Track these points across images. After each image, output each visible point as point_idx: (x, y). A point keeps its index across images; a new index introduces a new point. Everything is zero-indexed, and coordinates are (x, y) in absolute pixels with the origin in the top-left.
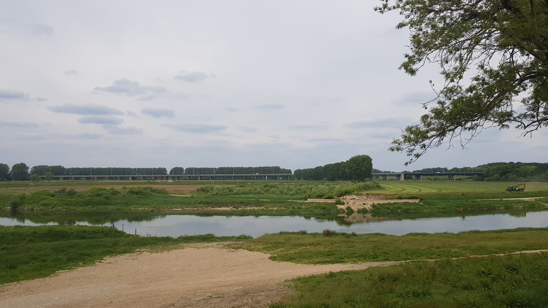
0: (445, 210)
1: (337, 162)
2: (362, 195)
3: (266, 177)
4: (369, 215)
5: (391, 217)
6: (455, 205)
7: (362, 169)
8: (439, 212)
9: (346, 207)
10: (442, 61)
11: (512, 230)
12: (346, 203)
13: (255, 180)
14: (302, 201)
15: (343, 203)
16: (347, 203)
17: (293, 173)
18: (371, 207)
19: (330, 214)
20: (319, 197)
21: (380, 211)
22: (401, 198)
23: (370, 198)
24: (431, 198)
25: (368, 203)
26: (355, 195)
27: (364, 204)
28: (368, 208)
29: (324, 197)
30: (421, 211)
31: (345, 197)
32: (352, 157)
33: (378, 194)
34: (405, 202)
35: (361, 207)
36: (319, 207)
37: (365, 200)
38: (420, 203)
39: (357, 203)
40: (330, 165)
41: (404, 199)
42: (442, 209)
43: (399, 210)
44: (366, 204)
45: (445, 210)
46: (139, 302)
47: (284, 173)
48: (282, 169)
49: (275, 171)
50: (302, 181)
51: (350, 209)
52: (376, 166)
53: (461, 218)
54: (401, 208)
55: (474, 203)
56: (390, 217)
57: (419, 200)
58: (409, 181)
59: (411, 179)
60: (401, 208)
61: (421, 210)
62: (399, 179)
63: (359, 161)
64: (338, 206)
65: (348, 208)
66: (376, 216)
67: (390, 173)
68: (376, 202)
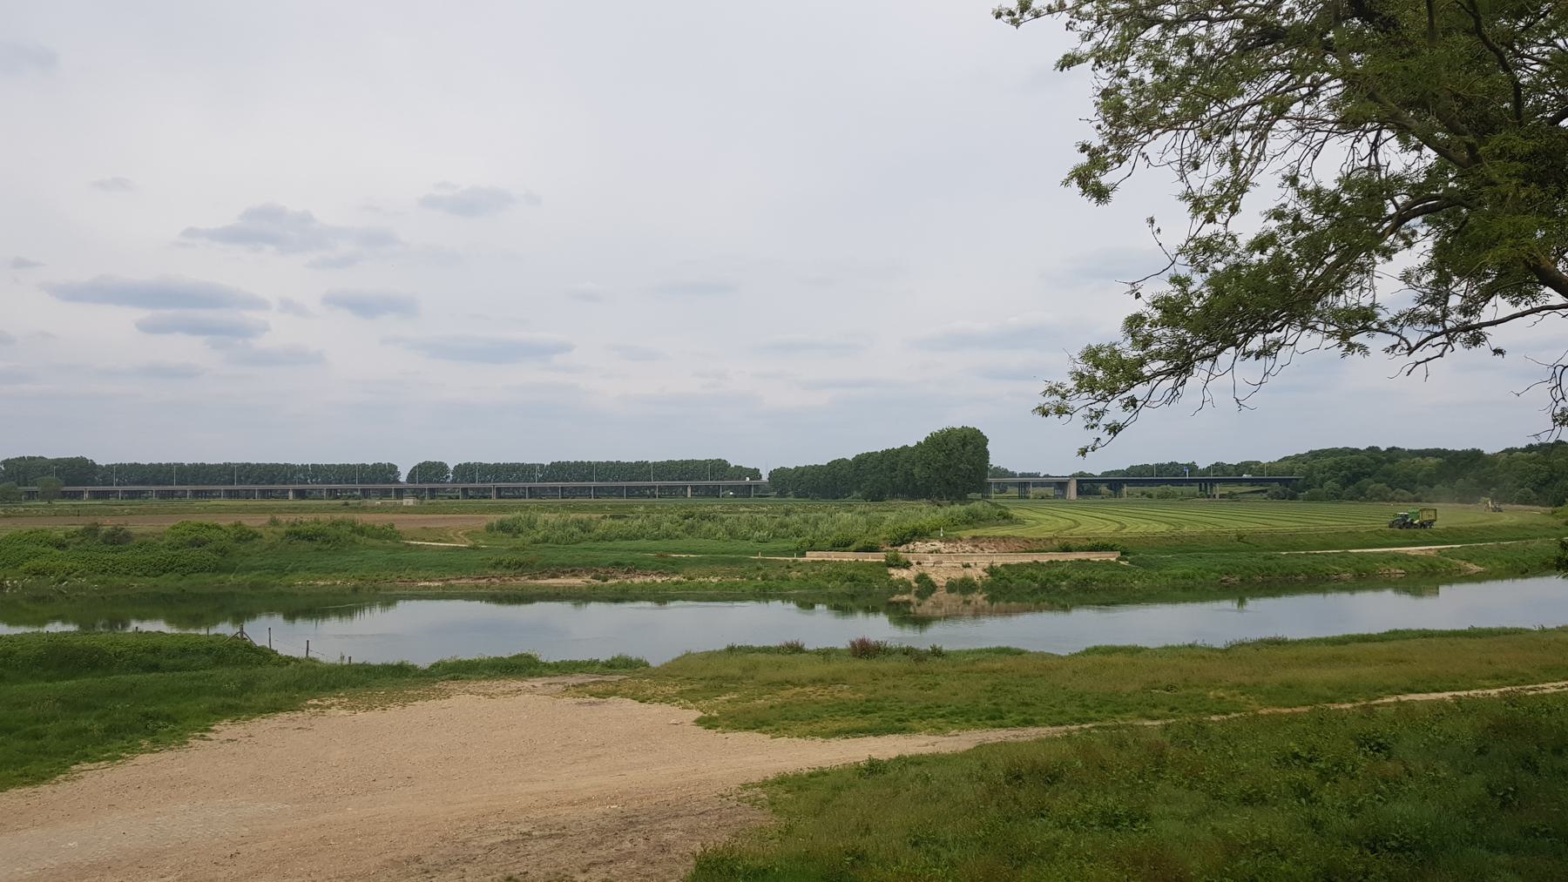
0: (1191, 583)
2: (961, 539)
3: (689, 490)
4: (978, 598)
7: (961, 466)
8: (1175, 588)
9: (916, 574)
12: (914, 562)
15: (908, 562)
16: (919, 563)
17: (765, 478)
18: (986, 574)
19: (870, 595)
20: (839, 546)
22: (1067, 549)
23: (982, 549)
25: (976, 564)
28: (975, 578)
29: (852, 547)
31: (911, 546)
33: (1004, 537)
34: (1079, 560)
35: (958, 575)
37: (968, 554)
38: (1122, 563)
39: (946, 563)
40: (869, 455)
41: (1077, 550)
42: (1183, 578)
43: (1064, 583)
44: (969, 567)
48: (732, 466)
50: (791, 501)
52: (1001, 456)
54: (1067, 577)
55: (1270, 563)
57: (1118, 554)
59: (1095, 494)
60: (1067, 577)
61: (1124, 581)
62: (1063, 496)
64: (892, 571)
65: (921, 578)
66: (998, 600)
68: (999, 561)
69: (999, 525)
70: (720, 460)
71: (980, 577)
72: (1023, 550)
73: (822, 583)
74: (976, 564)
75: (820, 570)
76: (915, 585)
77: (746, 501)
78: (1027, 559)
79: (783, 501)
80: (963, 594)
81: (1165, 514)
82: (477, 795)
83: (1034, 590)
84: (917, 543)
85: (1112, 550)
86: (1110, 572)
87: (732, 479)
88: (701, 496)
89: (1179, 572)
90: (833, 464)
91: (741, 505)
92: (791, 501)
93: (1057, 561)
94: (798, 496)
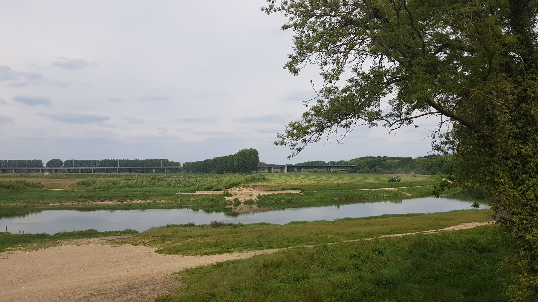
0: (323, 200)
1: (226, 156)
3: (154, 170)
4: (255, 206)
6: (331, 195)
7: (249, 162)
8: (318, 202)
12: (233, 194)
14: (190, 194)
15: (231, 194)
16: (235, 195)
17: (182, 166)
18: (257, 198)
20: (207, 189)
21: (265, 201)
23: (256, 190)
25: (254, 195)
26: (243, 187)
27: (250, 196)
29: (212, 189)
30: (302, 201)
31: (232, 189)
32: (240, 151)
33: (263, 186)
35: (248, 199)
36: (208, 199)
37: (251, 191)
38: (301, 194)
39: (244, 195)
40: (218, 158)
42: (321, 198)
43: (283, 201)
47: (172, 166)
50: (191, 174)
52: (262, 159)
54: (284, 199)
55: (347, 193)
57: (300, 191)
60: (284, 199)
62: (283, 172)
63: (246, 155)
64: (226, 197)
65: (236, 200)
66: (261, 207)
68: (262, 194)
69: (262, 182)
70: (165, 159)
72: (270, 190)
74: (254, 195)
75: (201, 197)
76: (234, 202)
77: (175, 174)
78: (271, 193)
83: (273, 203)
84: (234, 188)
85: (298, 190)
86: (298, 197)
88: (158, 172)
89: (319, 197)
92: (191, 174)
94: (193, 172)
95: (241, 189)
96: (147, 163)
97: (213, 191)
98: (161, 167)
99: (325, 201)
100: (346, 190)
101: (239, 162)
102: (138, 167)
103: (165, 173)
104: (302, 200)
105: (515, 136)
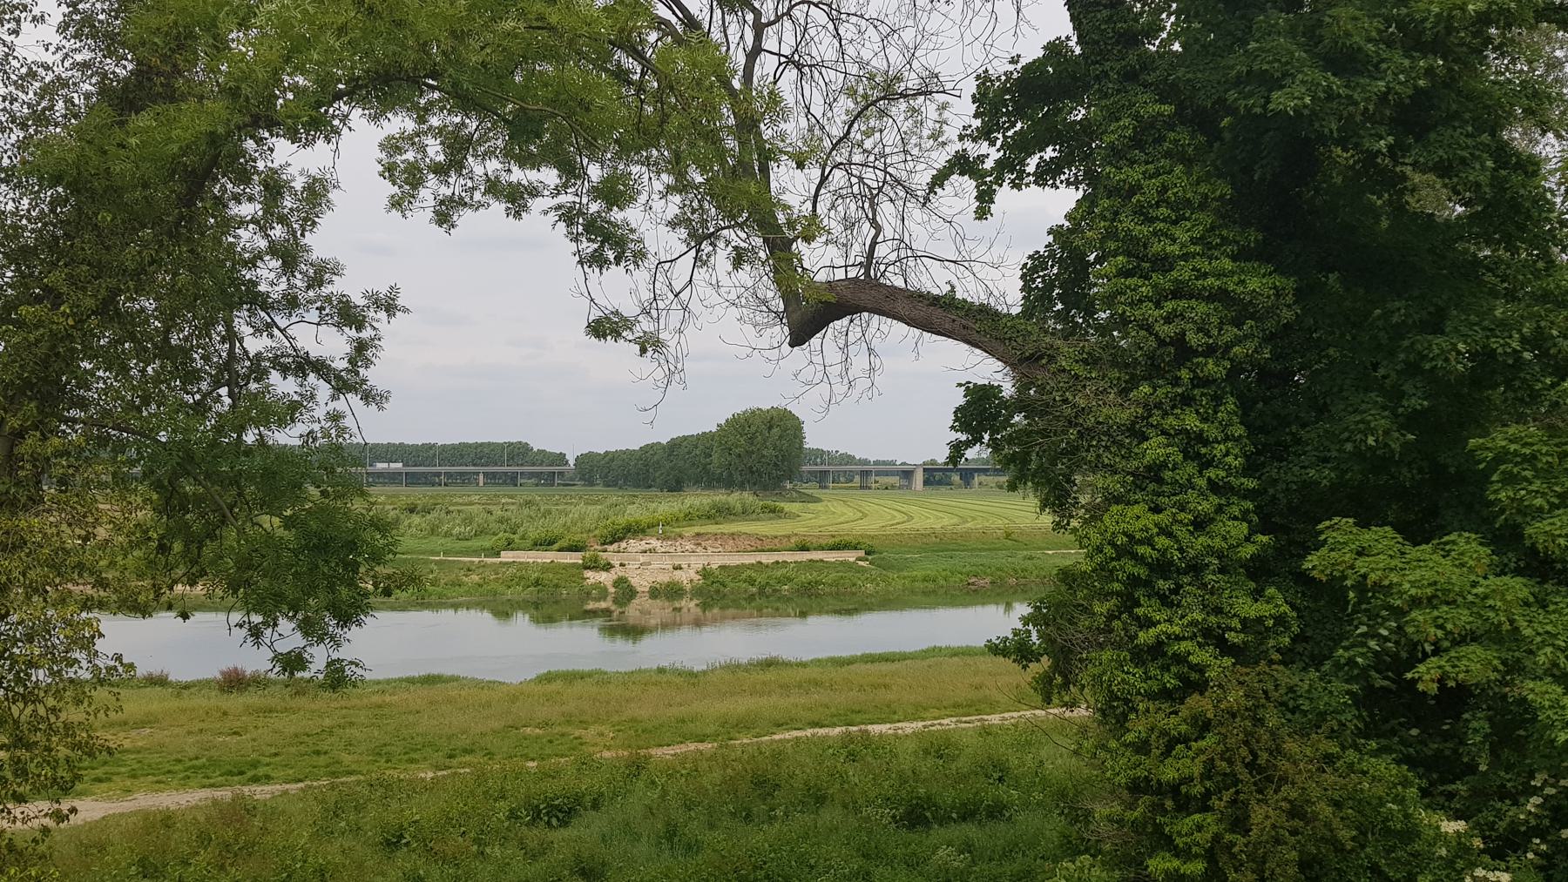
0: (931, 586)
1: (707, 431)
2: (681, 536)
3: (481, 477)
4: (690, 605)
5: (765, 610)
6: (968, 568)
9: (615, 577)
10: (908, 66)
11: (515, 695)
12: (616, 563)
13: (443, 487)
14: (476, 560)
15: (609, 564)
16: (622, 565)
17: (572, 462)
19: (556, 602)
20: (541, 545)
21: (722, 589)
23: (705, 548)
24: (904, 546)
27: (675, 568)
28: (685, 582)
29: (556, 546)
30: (854, 589)
31: (623, 545)
33: (733, 534)
35: (664, 578)
36: (522, 578)
38: (860, 563)
40: (685, 438)
42: (924, 580)
43: (786, 587)
44: (681, 568)
45: (931, 586)
46: (738, 793)
47: (541, 465)
49: (513, 458)
50: (599, 491)
51: (626, 585)
52: (813, 439)
53: (1001, 608)
56: (759, 610)
57: (861, 553)
58: (943, 489)
60: (790, 580)
61: (854, 585)
62: (909, 487)
63: (753, 429)
64: (589, 574)
65: (621, 582)
66: (711, 607)
67: (894, 464)
68: (716, 562)
71: (691, 581)
72: (754, 549)
73: (501, 589)
76: (613, 590)
77: (548, 490)
79: (592, 491)
80: (306, 634)
81: (976, 507)
82: (462, 771)
85: (856, 549)
87: (533, 465)
89: (919, 574)
90: (646, 449)
91: (504, 496)
92: (599, 491)
93: (785, 562)
95: (650, 546)
96: (462, 456)
97: (559, 551)
98: (505, 469)
99: (942, 591)
100: (1025, 553)
101: (730, 454)
102: (465, 468)
103: (519, 488)
104: (854, 585)
105: (41, 264)
